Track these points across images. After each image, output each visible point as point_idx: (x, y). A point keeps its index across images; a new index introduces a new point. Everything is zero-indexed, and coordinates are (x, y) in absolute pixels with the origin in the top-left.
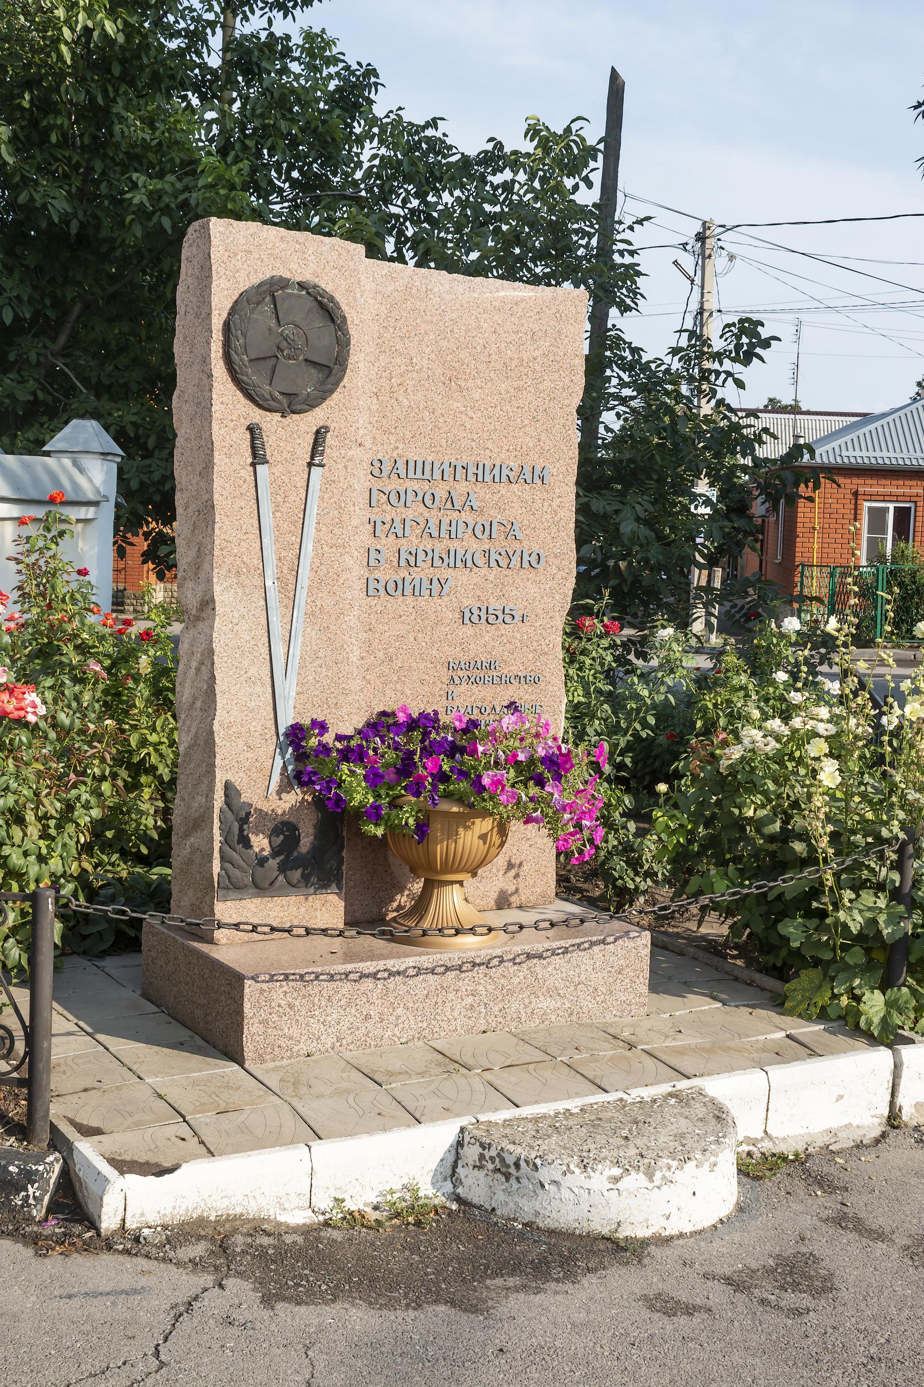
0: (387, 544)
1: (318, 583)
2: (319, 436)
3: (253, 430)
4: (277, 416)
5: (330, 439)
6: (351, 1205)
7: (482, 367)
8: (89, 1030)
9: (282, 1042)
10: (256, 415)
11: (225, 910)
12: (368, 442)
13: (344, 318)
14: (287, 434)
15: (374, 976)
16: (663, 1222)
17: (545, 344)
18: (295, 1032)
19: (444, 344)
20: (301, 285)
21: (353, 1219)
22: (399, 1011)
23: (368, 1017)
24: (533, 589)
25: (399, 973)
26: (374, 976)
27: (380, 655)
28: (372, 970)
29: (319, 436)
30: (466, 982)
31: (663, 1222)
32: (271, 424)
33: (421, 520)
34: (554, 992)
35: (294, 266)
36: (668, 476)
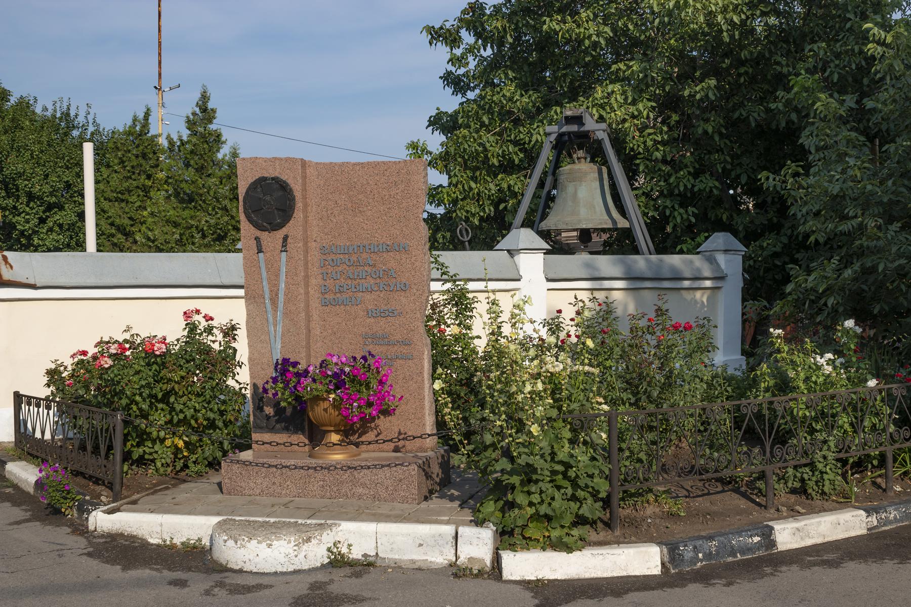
0: (330, 283)
1: (287, 301)
2: (285, 238)
3: (257, 239)
4: (267, 233)
5: (289, 240)
6: (174, 541)
7: (371, 201)
8: (873, 531)
9: (238, 488)
10: (258, 233)
11: (255, 436)
12: (318, 240)
13: (291, 190)
14: (272, 240)
15: (276, 466)
16: (243, 564)
17: (402, 187)
18: (243, 484)
19: (351, 193)
20: (273, 179)
21: (173, 546)
22: (288, 483)
23: (274, 483)
24: (404, 300)
25: (273, 466)
26: (276, 466)
27: (330, 331)
28: (275, 464)
29: (285, 238)
30: (319, 475)
31: (243, 564)
32: (264, 236)
33: (345, 271)
34: (364, 485)
35: (271, 171)
36: (735, 189)
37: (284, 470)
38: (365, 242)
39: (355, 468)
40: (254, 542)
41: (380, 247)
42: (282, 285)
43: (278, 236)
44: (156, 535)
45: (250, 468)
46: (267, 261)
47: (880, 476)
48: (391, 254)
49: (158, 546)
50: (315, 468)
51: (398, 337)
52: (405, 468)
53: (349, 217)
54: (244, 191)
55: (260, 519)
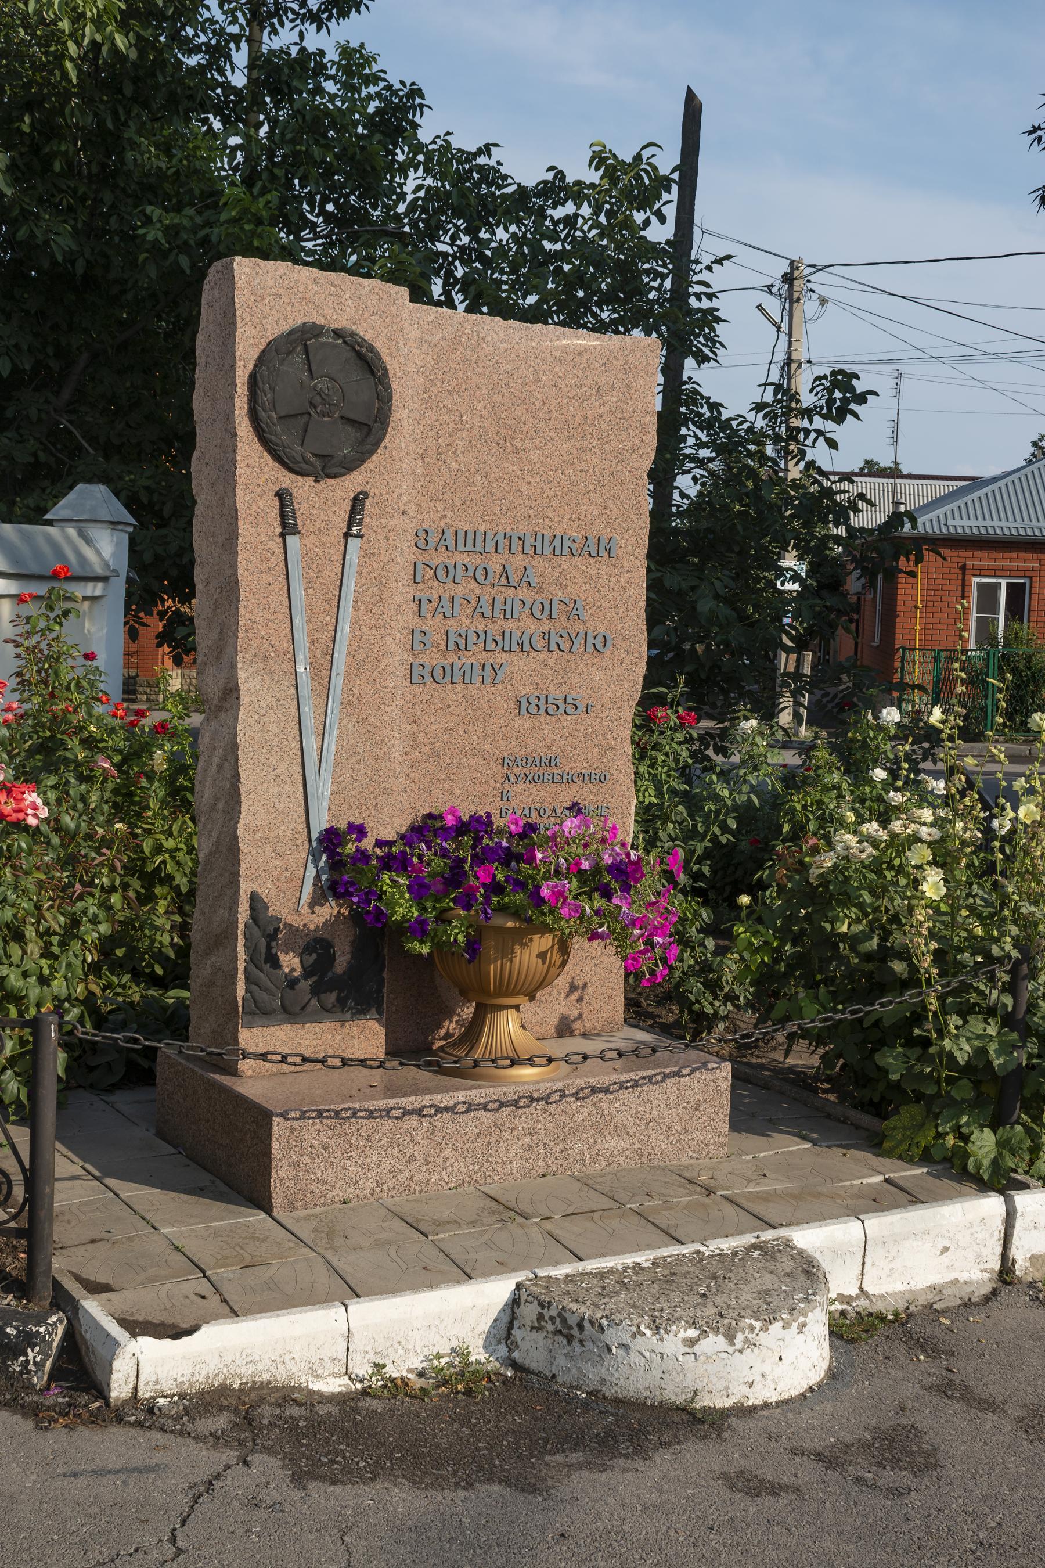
0: (433, 625)
1: (355, 669)
2: (357, 503)
3: (282, 496)
4: (309, 481)
6: (393, 1371)
7: (540, 425)
9: (316, 1187)
10: (287, 480)
11: (250, 1038)
12: (412, 510)
14: (321, 501)
16: (745, 1390)
17: (612, 399)
18: (329, 1175)
19: (499, 399)
20: (337, 333)
21: (395, 1387)
22: (447, 1152)
23: (412, 1159)
24: (598, 676)
27: (426, 750)
29: (357, 503)
30: (522, 1120)
32: (302, 487)
34: (621, 1131)
35: (329, 312)
37: (439, 1120)
38: (522, 529)
39: (606, 1091)
40: (776, 1327)
41: (557, 543)
42: (345, 628)
43: (339, 493)
44: (330, 1367)
45: (350, 1127)
46: (367, 555)
47: (713, 987)
48: (578, 561)
49: (341, 1399)
50: (515, 1104)
51: (580, 765)
52: (710, 1076)
53: (491, 461)
54: (254, 355)
55: (644, 1258)
